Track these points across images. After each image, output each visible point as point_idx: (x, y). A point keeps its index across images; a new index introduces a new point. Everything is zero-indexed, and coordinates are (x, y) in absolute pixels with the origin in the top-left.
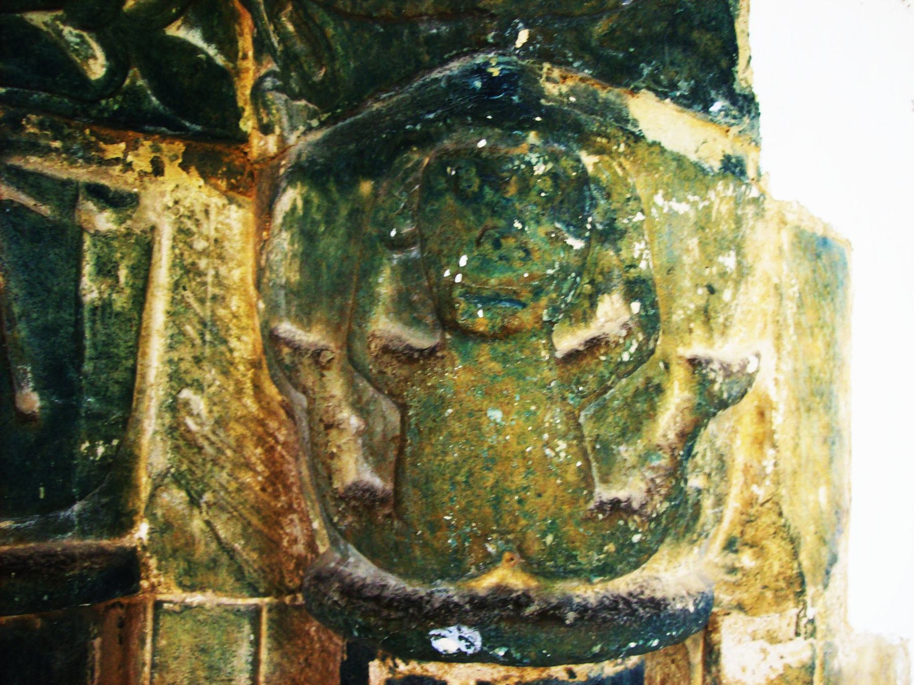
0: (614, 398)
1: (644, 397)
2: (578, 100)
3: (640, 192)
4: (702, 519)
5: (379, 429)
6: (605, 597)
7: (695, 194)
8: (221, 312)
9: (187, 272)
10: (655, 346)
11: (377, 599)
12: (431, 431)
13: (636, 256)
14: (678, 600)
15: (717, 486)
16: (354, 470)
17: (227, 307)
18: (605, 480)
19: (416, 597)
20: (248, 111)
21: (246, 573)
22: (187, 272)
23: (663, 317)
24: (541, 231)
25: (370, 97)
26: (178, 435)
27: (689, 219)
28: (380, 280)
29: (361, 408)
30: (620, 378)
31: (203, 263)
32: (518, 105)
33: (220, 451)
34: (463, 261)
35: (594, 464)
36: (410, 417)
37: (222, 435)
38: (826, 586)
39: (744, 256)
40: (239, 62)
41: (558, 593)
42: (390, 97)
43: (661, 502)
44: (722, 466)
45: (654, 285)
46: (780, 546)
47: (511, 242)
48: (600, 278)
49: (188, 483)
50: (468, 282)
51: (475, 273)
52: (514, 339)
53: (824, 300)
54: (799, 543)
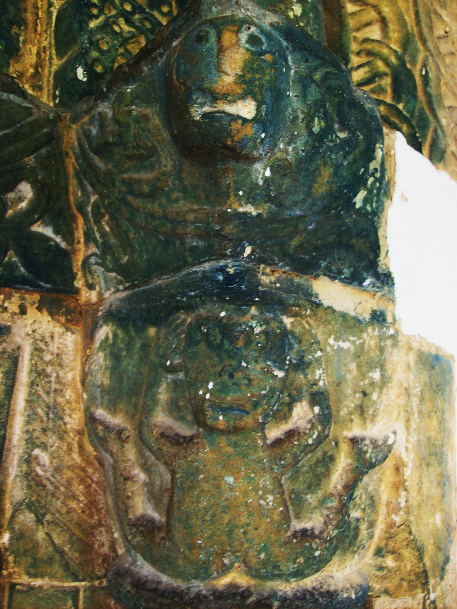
0: (303, 465)
1: (322, 464)
2: (281, 285)
3: (320, 337)
4: (360, 538)
5: (158, 482)
6: (298, 591)
7: (354, 336)
8: (60, 400)
9: (39, 375)
10: (329, 432)
11: (155, 590)
12: (190, 488)
13: (317, 378)
14: (344, 591)
15: (369, 516)
16: (141, 506)
17: (64, 396)
18: (298, 517)
19: (179, 590)
20: (80, 274)
21: (71, 567)
22: (39, 375)
23: (334, 413)
24: (258, 367)
25: (155, 277)
26: (30, 478)
27: (350, 351)
28: (160, 390)
29: (147, 469)
30: (306, 454)
31: (49, 369)
32: (245, 291)
33: (57, 488)
34: (211, 385)
35: (291, 508)
36: (177, 479)
37: (58, 478)
38: (442, 578)
39: (386, 371)
40: (75, 246)
41: (268, 589)
42: (168, 278)
43: (333, 530)
44: (373, 503)
45: (328, 395)
46: (410, 553)
47: (239, 375)
48: (295, 393)
49: (36, 509)
50: (213, 399)
51: (218, 394)
52: (242, 433)
53: (437, 394)
54: (423, 551)
